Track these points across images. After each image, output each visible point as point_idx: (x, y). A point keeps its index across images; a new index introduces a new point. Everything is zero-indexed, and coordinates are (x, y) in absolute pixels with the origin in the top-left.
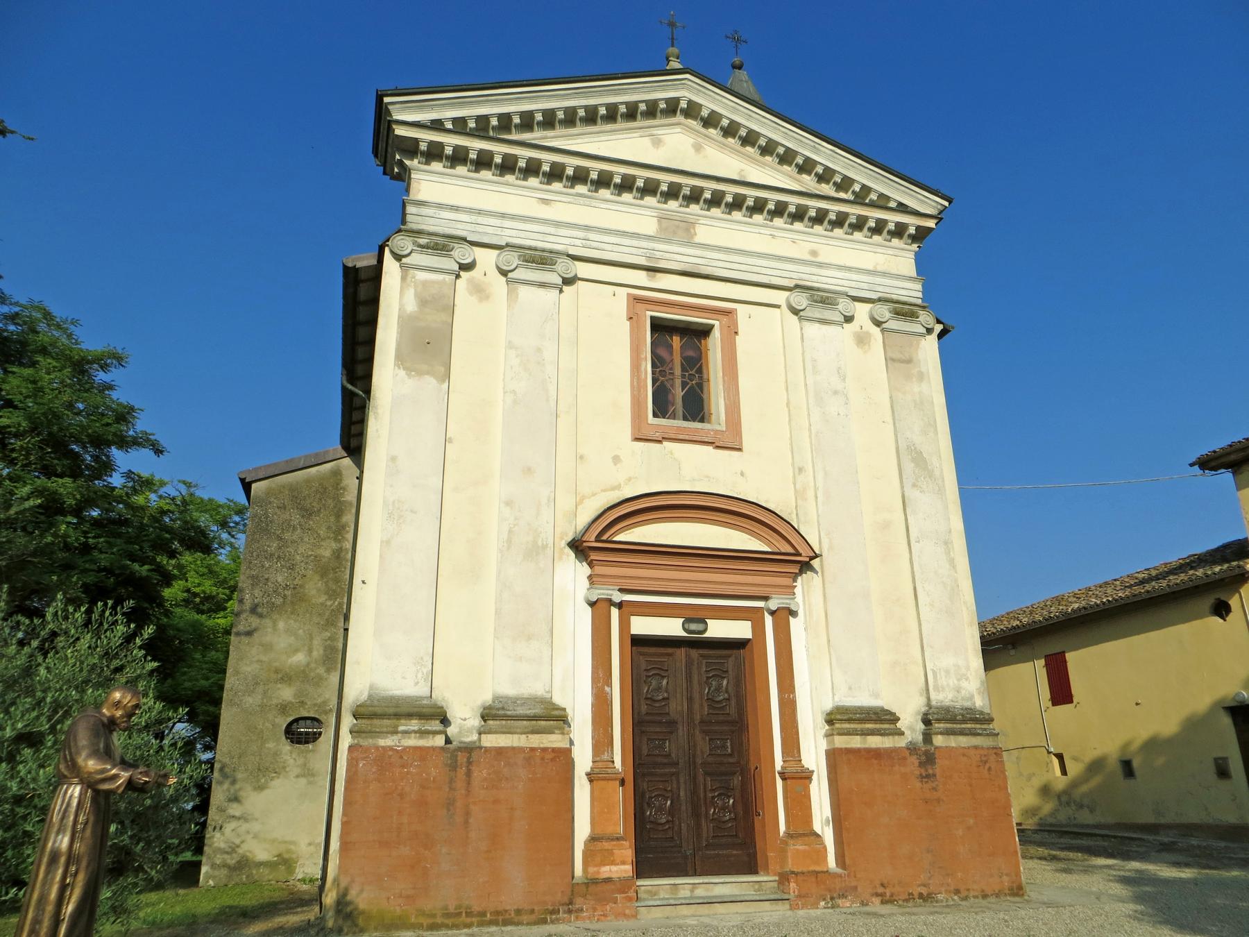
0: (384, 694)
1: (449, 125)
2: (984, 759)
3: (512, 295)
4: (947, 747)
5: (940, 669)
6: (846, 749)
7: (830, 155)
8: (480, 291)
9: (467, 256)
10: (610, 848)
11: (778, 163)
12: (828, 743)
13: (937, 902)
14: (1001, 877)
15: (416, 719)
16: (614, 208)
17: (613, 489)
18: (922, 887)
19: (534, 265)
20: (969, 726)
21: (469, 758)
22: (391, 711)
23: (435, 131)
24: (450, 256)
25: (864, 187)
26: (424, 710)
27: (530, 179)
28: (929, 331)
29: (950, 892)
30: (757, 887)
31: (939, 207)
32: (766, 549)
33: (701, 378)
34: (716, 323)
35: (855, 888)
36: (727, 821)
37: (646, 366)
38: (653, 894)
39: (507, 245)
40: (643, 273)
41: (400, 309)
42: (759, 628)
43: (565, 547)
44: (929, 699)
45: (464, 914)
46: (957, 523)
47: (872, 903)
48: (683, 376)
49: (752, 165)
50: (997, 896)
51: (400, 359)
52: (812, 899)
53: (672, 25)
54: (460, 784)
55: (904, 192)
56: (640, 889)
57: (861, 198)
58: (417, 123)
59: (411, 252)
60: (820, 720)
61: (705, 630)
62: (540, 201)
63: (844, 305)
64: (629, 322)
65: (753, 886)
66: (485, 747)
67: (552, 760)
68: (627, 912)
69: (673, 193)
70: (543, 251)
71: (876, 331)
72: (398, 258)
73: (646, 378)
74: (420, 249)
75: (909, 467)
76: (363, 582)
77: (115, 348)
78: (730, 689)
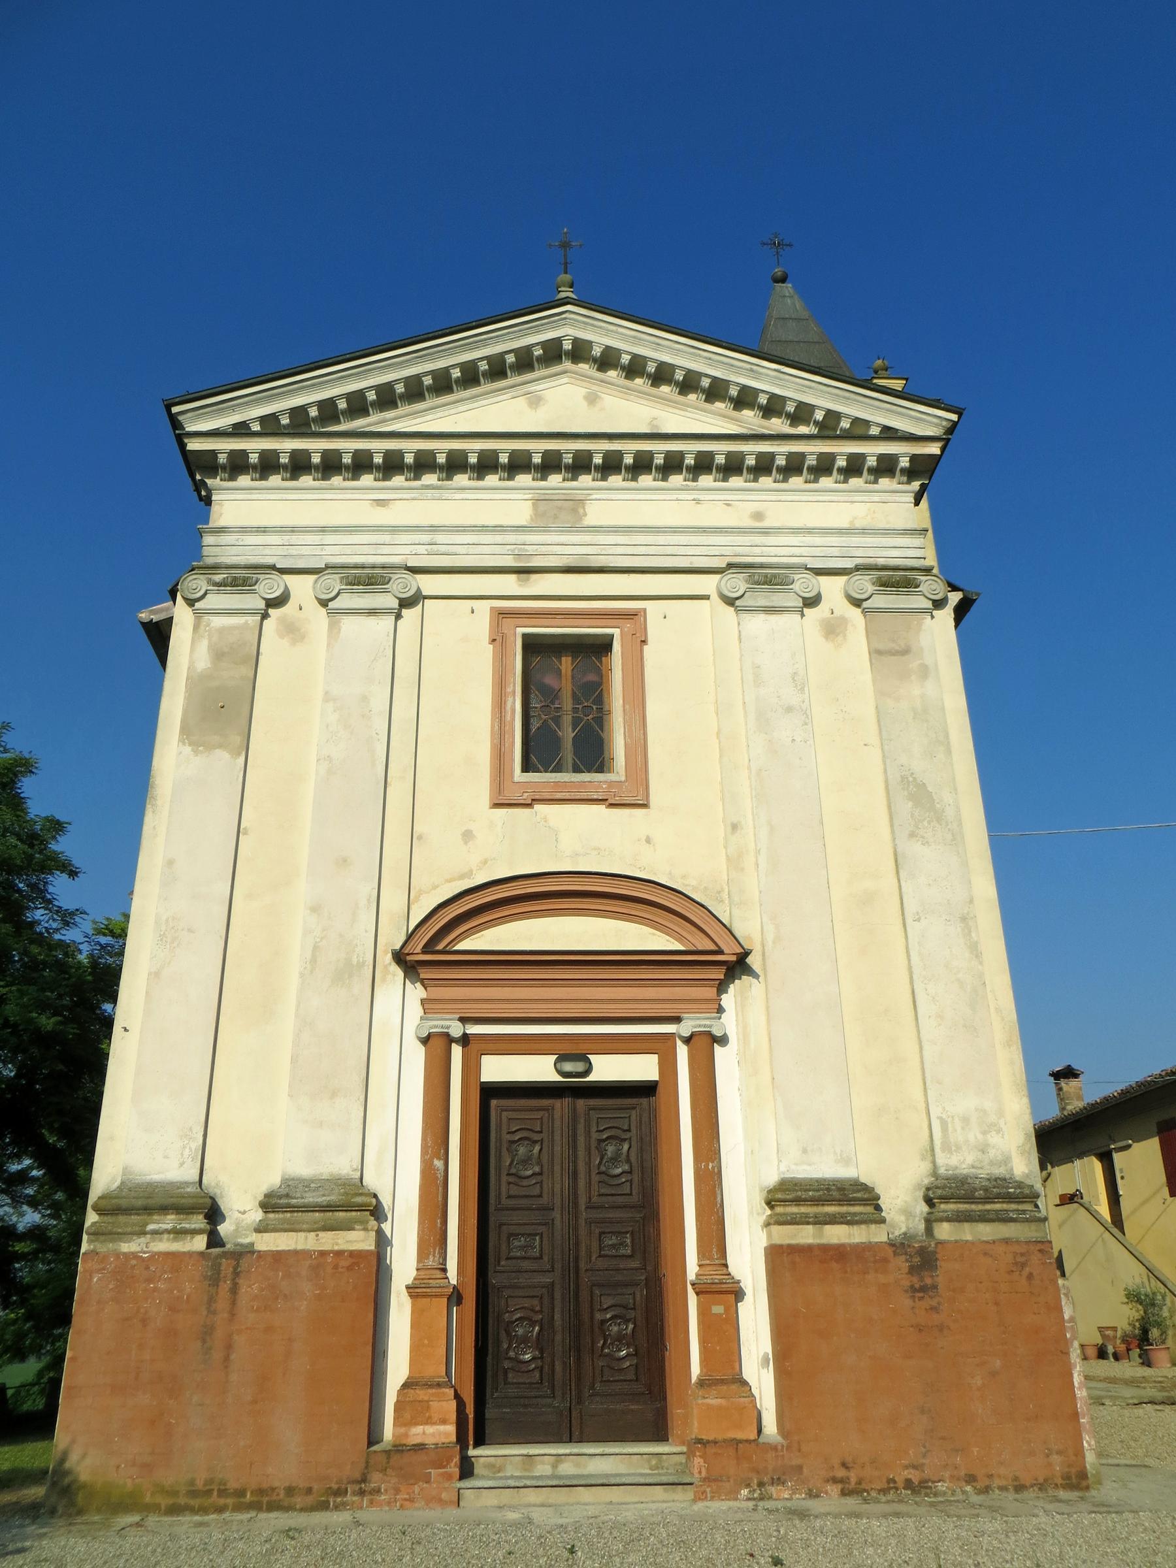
0: (139, 1179)
1: (256, 427)
2: (1022, 1259)
3: (333, 627)
4: (956, 1241)
5: (953, 1117)
6: (790, 1246)
7: (776, 377)
8: (292, 631)
9: (275, 588)
10: (426, 1398)
11: (706, 401)
12: (769, 1236)
13: (935, 1495)
14: (1048, 1456)
15: (172, 1214)
16: (789, 498)
17: (462, 877)
18: (912, 1471)
19: (361, 587)
20: (998, 1206)
21: (235, 1268)
22: (139, 1203)
23: (267, 437)
24: (253, 592)
25: (829, 413)
26: (183, 1201)
27: (760, 479)
28: (939, 604)
29: (958, 1479)
30: (654, 1462)
31: (944, 423)
32: (678, 946)
33: (600, 710)
34: (616, 632)
35: (800, 1468)
36: (623, 1358)
37: (514, 703)
38: (496, 1469)
39: (327, 567)
40: (513, 577)
41: (189, 668)
42: (668, 1066)
43: (390, 964)
44: (934, 1162)
45: (215, 1493)
46: (985, 887)
47: (826, 1493)
48: (575, 710)
49: (671, 410)
50: (1042, 1487)
51: (186, 731)
52: (727, 1485)
53: (565, 245)
54: (222, 1304)
55: (888, 410)
56: (477, 1461)
57: (829, 427)
58: (215, 432)
59: (205, 594)
60: (759, 1200)
61: (588, 1071)
62: (374, 503)
63: (804, 584)
64: (491, 646)
65: (649, 1461)
66: (260, 1251)
67: (350, 1268)
68: (444, 1496)
69: (550, 465)
70: (373, 567)
71: (855, 613)
72: (191, 602)
73: (513, 719)
74: (217, 588)
75: (905, 807)
76: (126, 1030)
77: (21, 752)
78: (633, 1159)
